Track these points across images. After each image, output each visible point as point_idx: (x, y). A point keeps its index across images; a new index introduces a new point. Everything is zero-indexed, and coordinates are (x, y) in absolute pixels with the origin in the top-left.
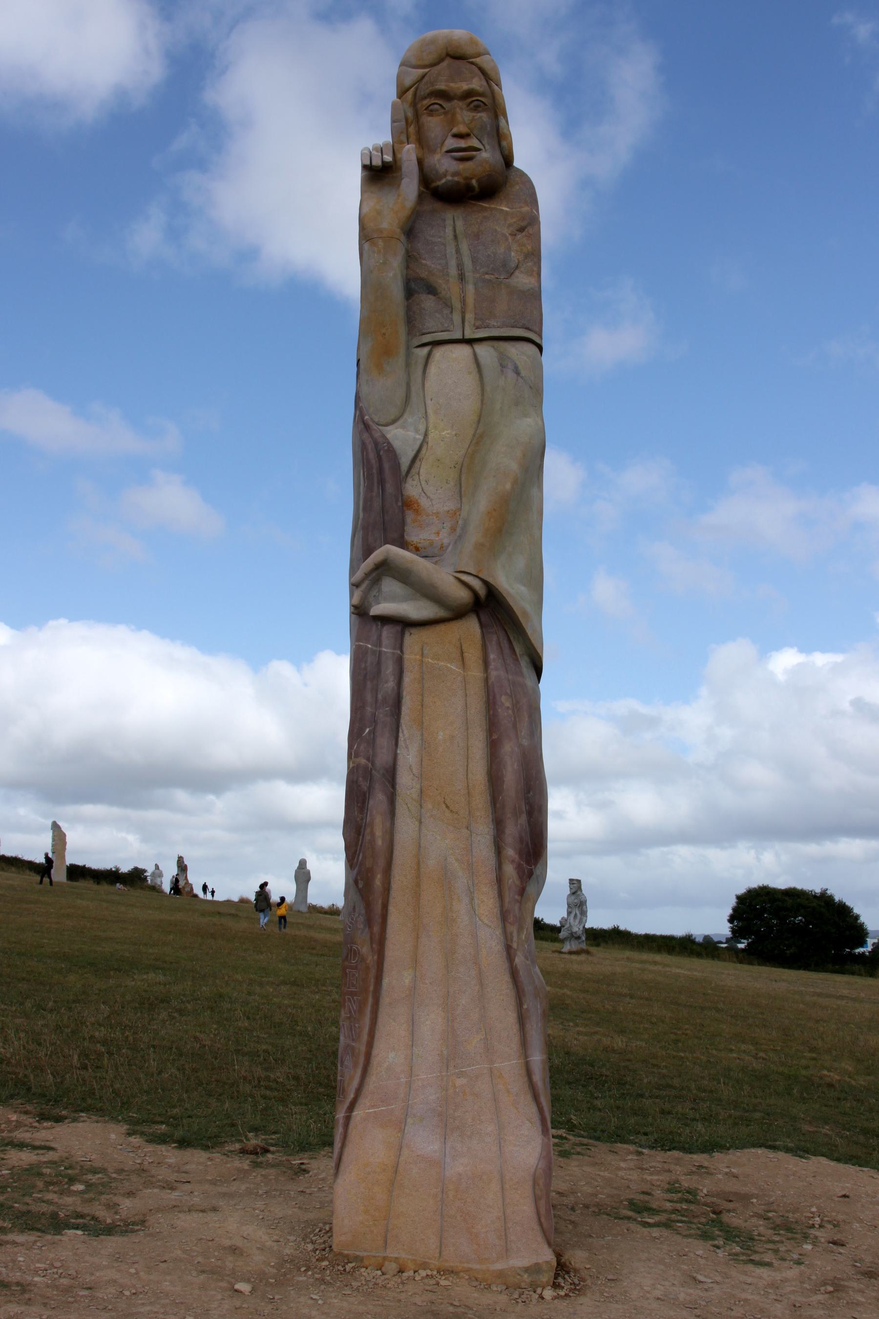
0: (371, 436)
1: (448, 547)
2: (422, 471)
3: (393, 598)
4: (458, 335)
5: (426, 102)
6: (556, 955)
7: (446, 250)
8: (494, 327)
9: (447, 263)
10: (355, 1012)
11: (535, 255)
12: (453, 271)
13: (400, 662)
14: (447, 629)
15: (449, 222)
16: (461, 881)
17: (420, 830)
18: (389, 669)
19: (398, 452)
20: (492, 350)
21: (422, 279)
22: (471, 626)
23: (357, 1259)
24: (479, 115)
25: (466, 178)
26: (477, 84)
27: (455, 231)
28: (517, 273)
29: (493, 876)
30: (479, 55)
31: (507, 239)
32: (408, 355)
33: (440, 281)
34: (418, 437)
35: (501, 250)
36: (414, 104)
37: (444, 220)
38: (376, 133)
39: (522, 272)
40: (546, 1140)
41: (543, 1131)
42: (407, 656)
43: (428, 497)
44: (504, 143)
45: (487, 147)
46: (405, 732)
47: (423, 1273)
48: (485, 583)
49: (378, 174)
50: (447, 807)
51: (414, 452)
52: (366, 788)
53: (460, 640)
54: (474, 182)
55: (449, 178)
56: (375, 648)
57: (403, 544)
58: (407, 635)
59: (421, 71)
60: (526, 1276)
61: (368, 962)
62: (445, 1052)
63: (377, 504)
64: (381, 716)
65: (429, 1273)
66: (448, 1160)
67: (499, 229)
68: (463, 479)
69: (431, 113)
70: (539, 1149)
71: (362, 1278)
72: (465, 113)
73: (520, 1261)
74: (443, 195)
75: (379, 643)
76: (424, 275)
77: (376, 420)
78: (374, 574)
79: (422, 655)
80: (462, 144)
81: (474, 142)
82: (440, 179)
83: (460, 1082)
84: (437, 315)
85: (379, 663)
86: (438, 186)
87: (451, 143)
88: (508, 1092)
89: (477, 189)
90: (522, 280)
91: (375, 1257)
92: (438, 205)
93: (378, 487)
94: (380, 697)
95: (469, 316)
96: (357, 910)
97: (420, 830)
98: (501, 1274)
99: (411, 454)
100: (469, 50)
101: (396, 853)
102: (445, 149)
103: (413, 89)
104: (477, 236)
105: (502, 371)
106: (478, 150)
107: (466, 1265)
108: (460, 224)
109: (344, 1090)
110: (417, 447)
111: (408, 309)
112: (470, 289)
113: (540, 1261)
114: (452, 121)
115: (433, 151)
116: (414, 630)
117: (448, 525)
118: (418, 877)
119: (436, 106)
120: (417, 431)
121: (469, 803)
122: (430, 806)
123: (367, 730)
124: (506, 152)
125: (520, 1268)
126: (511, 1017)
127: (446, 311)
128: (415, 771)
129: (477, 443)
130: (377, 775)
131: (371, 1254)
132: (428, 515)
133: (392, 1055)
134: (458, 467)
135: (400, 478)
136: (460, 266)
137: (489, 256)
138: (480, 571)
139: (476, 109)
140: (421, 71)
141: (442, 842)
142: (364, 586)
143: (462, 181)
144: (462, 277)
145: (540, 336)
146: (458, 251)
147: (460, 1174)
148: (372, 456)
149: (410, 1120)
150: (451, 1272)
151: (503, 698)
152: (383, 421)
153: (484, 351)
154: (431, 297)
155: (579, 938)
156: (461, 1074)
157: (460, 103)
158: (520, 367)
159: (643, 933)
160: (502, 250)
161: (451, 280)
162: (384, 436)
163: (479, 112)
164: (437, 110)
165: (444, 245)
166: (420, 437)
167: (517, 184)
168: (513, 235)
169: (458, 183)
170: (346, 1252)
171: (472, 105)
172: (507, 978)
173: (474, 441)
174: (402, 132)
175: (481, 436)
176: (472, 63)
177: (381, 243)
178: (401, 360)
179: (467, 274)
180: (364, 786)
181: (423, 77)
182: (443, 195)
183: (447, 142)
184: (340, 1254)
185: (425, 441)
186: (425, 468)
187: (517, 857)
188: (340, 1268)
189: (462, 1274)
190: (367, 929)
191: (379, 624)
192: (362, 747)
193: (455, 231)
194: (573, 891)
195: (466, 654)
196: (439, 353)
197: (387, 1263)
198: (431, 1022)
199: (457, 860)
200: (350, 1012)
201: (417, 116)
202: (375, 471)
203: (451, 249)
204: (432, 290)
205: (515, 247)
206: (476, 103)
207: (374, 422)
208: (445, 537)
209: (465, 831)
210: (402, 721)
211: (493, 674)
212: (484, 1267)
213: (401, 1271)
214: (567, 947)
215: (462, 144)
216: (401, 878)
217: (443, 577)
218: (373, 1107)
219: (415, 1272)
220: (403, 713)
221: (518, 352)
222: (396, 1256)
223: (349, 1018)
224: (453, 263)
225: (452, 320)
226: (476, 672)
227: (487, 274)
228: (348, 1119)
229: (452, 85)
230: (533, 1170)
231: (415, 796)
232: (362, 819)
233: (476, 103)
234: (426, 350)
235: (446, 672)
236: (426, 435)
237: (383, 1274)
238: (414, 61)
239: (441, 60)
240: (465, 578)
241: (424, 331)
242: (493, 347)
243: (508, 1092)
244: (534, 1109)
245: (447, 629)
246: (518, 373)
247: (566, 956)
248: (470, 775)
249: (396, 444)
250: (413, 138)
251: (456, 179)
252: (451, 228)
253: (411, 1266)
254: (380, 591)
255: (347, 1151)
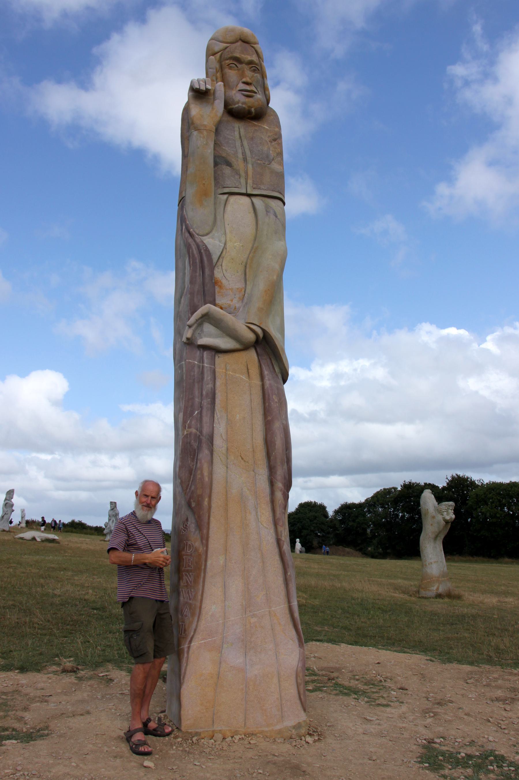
0: (195, 241)
2: (223, 264)
3: (210, 335)
4: (244, 191)
5: (228, 62)
7: (235, 144)
8: (263, 189)
9: (237, 151)
10: (191, 582)
11: (280, 154)
12: (240, 156)
13: (214, 372)
14: (229, 355)
15: (237, 129)
17: (227, 472)
18: (207, 376)
19: (211, 252)
20: (261, 202)
21: (223, 157)
23: (197, 734)
24: (256, 75)
25: (249, 107)
26: (254, 58)
27: (240, 134)
28: (273, 162)
29: (268, 499)
30: (255, 43)
32: (215, 198)
33: (233, 160)
35: (265, 149)
37: (234, 127)
38: (198, 73)
40: (302, 650)
41: (299, 645)
44: (267, 92)
45: (260, 93)
47: (237, 737)
48: (264, 331)
49: (199, 94)
50: (242, 459)
52: (196, 447)
53: (246, 362)
54: (253, 110)
55: (240, 105)
57: (215, 304)
58: (217, 357)
59: (225, 45)
61: (200, 551)
62: (244, 603)
63: (199, 280)
64: (205, 404)
66: (248, 667)
68: (247, 270)
69: (231, 68)
70: (298, 656)
73: (290, 722)
75: (202, 360)
76: (224, 155)
77: (197, 232)
78: (200, 321)
80: (248, 88)
81: (253, 88)
82: (235, 105)
83: (253, 620)
84: (232, 178)
85: (202, 373)
87: (242, 86)
88: (280, 624)
89: (253, 114)
90: (275, 166)
91: (207, 731)
92: (230, 119)
94: (204, 393)
95: (250, 181)
97: (227, 472)
98: (280, 732)
99: (219, 254)
100: (252, 40)
101: (214, 486)
102: (238, 89)
103: (220, 53)
104: (252, 139)
105: (267, 214)
106: (256, 93)
107: (260, 729)
108: (242, 131)
109: (185, 630)
110: (221, 250)
111: (215, 172)
112: (250, 166)
113: (301, 721)
116: (220, 355)
118: (227, 500)
119: (234, 65)
120: (220, 241)
122: (233, 458)
123: (196, 412)
124: (268, 98)
125: (290, 727)
126: (280, 580)
127: (237, 177)
128: (224, 437)
129: (255, 252)
130: (204, 439)
132: (227, 290)
133: (214, 607)
134: (244, 264)
135: (212, 268)
136: (244, 153)
137: (259, 151)
139: (254, 71)
140: (225, 45)
141: (234, 477)
143: (246, 107)
144: (245, 160)
145: (284, 196)
146: (242, 145)
149: (225, 646)
151: (274, 397)
152: (201, 233)
153: (257, 201)
154: (229, 167)
156: (254, 616)
157: (246, 66)
158: (277, 214)
160: (266, 149)
161: (239, 160)
162: (202, 242)
164: (234, 67)
165: (235, 140)
166: (223, 245)
168: (271, 142)
169: (244, 108)
170: (190, 731)
172: (277, 558)
173: (253, 251)
175: (256, 248)
176: (253, 47)
177: (205, 133)
178: (212, 199)
179: (248, 158)
180: (195, 445)
181: (226, 48)
182: (234, 113)
183: (239, 85)
184: (187, 732)
185: (225, 248)
188: (190, 741)
189: (258, 735)
190: (197, 532)
192: (193, 422)
193: (240, 134)
194: (112, 508)
196: (233, 199)
197: (216, 735)
198: (236, 586)
199: (248, 489)
200: (187, 582)
201: (222, 68)
202: (198, 261)
203: (238, 144)
204: (229, 164)
205: (271, 148)
206: (254, 68)
207: (196, 233)
208: (236, 303)
210: (216, 408)
211: (267, 383)
212: (270, 729)
213: (224, 738)
215: (248, 88)
216: (217, 501)
217: (240, 326)
218: (203, 639)
219: (232, 737)
220: (216, 403)
222: (220, 729)
223: (187, 586)
224: (240, 151)
225: (240, 182)
226: (257, 382)
228: (189, 648)
229: (243, 55)
230: (295, 668)
231: (224, 452)
232: (193, 466)
233: (254, 68)
234: (225, 196)
235: (236, 379)
237: (215, 741)
238: (221, 39)
240: (252, 326)
241: (225, 186)
243: (280, 624)
244: (294, 632)
245: (229, 355)
246: (276, 217)
248: (254, 441)
249: (210, 247)
250: (219, 79)
251: (244, 106)
253: (229, 734)
254: (202, 331)
255: (188, 667)
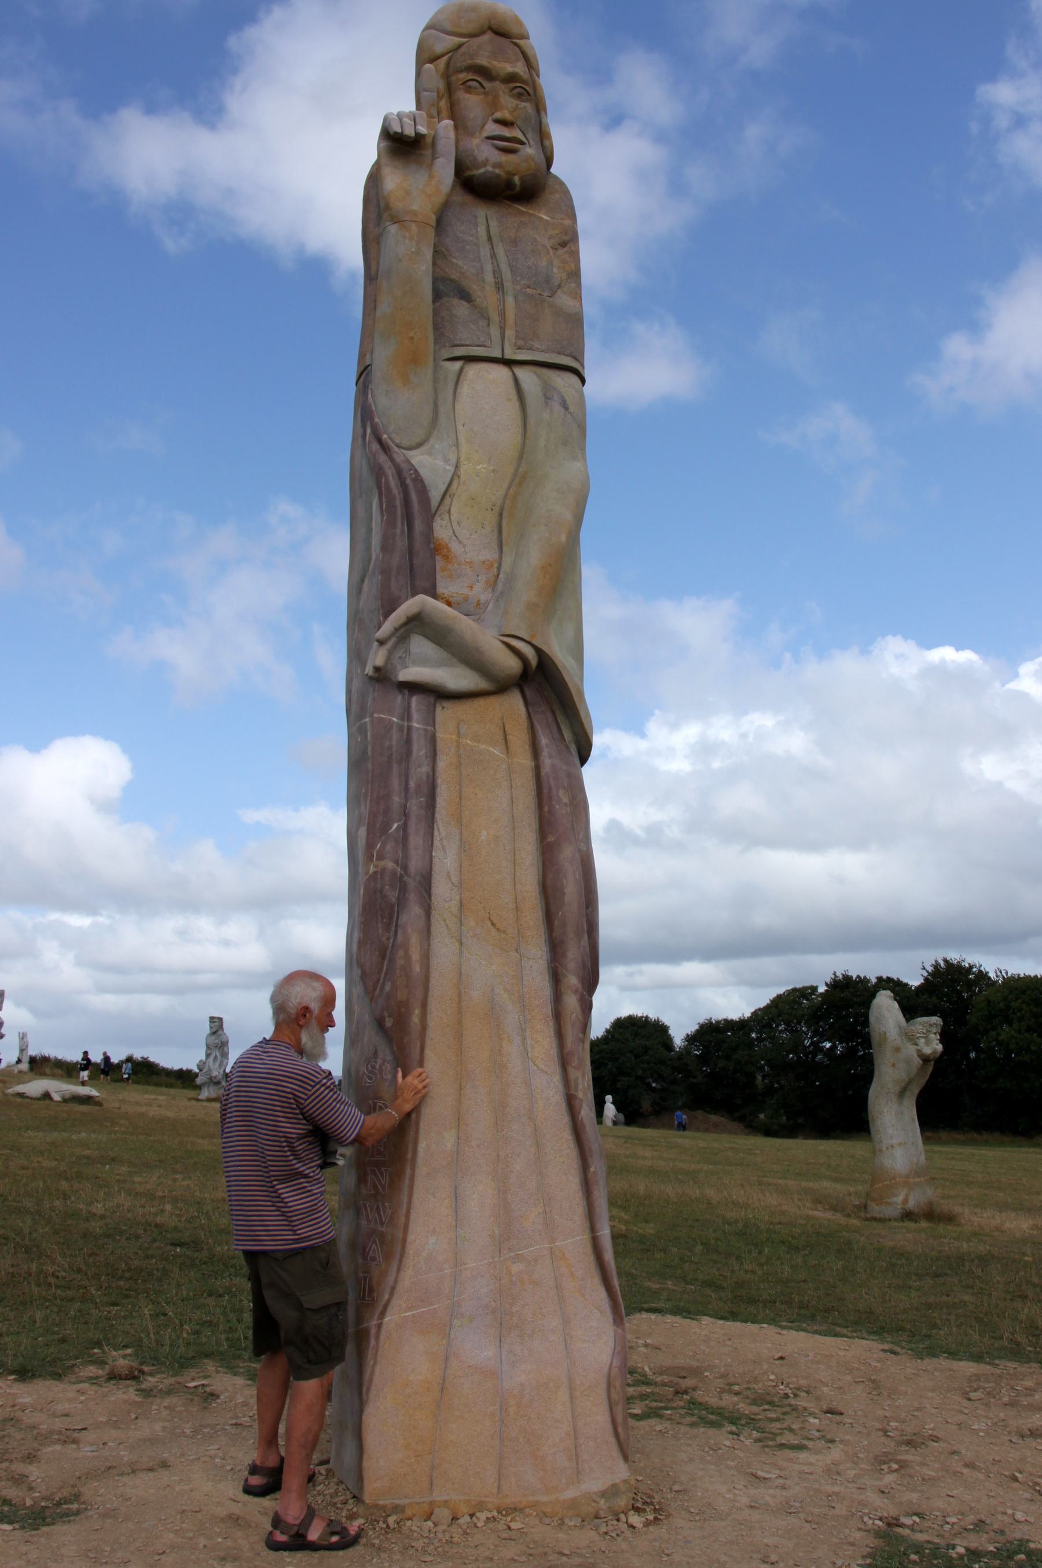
0: (392, 460)
1: (487, 603)
2: (453, 510)
3: (424, 662)
4: (497, 353)
5: (463, 76)
6: (194, 1103)
7: (479, 252)
8: (538, 350)
12: (489, 278)
13: (433, 740)
14: (465, 703)
15: (481, 220)
16: (512, 1018)
18: (419, 749)
19: (426, 482)
20: (535, 377)
21: (451, 280)
22: (514, 703)
23: (397, 1509)
24: (523, 104)
27: (488, 231)
29: (548, 1010)
31: (548, 253)
32: (436, 368)
34: (448, 467)
35: (543, 263)
36: (447, 76)
37: (476, 217)
39: (565, 293)
41: (615, 1321)
42: (439, 735)
43: (460, 542)
44: (546, 143)
46: (441, 830)
47: (482, 1516)
48: (539, 651)
49: (400, 145)
50: (493, 924)
51: (445, 486)
52: (394, 900)
53: (502, 718)
54: (516, 179)
55: (489, 168)
56: (401, 723)
57: (435, 596)
58: (438, 709)
59: (457, 40)
60: (602, 1502)
62: (497, 1232)
64: (414, 808)
65: (490, 1515)
67: (539, 239)
68: (504, 524)
69: (469, 90)
70: (611, 1344)
71: (415, 1534)
72: (508, 98)
73: (594, 1484)
74: (477, 187)
75: (407, 715)
76: (455, 275)
77: (397, 441)
79: (459, 734)
80: (506, 132)
81: (517, 133)
82: (478, 168)
83: (517, 1268)
84: (472, 325)
85: (408, 741)
86: (474, 176)
89: (518, 189)
90: (563, 300)
91: (419, 1503)
92: (468, 199)
93: (403, 524)
94: (412, 784)
95: (510, 333)
96: (381, 1055)
98: (573, 1504)
102: (485, 134)
103: (446, 58)
104: (515, 242)
105: (546, 403)
107: (531, 1498)
110: (448, 480)
111: (436, 313)
112: (510, 300)
113: (618, 1481)
114: (494, 104)
115: (472, 135)
116: (446, 704)
117: (483, 578)
118: (460, 1012)
120: (446, 461)
121: (518, 919)
122: (472, 923)
123: (395, 826)
126: (574, 1183)
127: (482, 323)
130: (412, 884)
131: (414, 1500)
133: (432, 1240)
134: (497, 509)
136: (497, 273)
137: (529, 267)
138: (533, 636)
139: (519, 96)
140: (457, 40)
141: (477, 965)
142: (389, 645)
143: (503, 174)
144: (500, 286)
146: (494, 256)
147: (522, 1385)
148: (393, 483)
150: (514, 1510)
151: (561, 792)
152: (405, 443)
154: (465, 303)
155: (218, 1083)
156: (519, 1258)
157: (503, 86)
158: (568, 402)
159: (176, 1067)
162: (408, 461)
163: (523, 101)
164: (476, 88)
167: (557, 192)
169: (498, 176)
170: (381, 1502)
171: (516, 91)
172: (567, 1135)
174: (433, 105)
176: (516, 44)
180: (393, 895)
181: (460, 46)
182: (477, 187)
185: (456, 475)
186: (457, 507)
187: (580, 986)
191: (407, 692)
192: (388, 847)
193: (488, 231)
195: (509, 737)
196: (473, 370)
197: (437, 1511)
198: (480, 1195)
199: (506, 990)
201: (450, 89)
202: (398, 503)
203: (485, 251)
204: (465, 296)
205: (556, 263)
208: (480, 592)
209: (514, 954)
210: (437, 816)
211: (547, 763)
213: (455, 1518)
214: (205, 1094)
215: (506, 132)
218: (410, 1309)
219: (472, 1516)
220: (438, 806)
221: (562, 381)
222: (445, 1498)
224: (489, 268)
226: (524, 760)
227: (529, 287)
229: (495, 63)
230: (606, 1369)
232: (388, 939)
233: (519, 90)
234: (458, 365)
236: (457, 467)
237: (436, 1525)
238: (449, 27)
239: (482, 33)
240: (515, 643)
242: (535, 373)
245: (465, 703)
246: (566, 408)
247: (205, 1104)
248: (518, 886)
249: (424, 473)
250: (445, 113)
251: (497, 171)
252: (484, 228)
253: (464, 1509)
254: (408, 652)
